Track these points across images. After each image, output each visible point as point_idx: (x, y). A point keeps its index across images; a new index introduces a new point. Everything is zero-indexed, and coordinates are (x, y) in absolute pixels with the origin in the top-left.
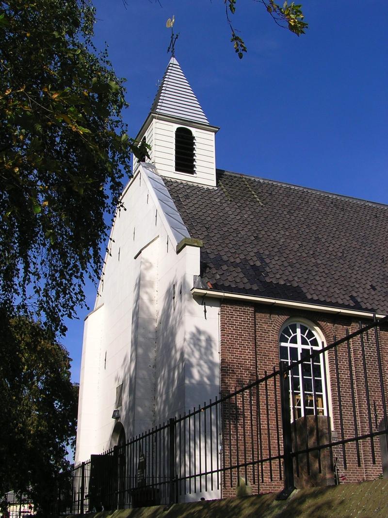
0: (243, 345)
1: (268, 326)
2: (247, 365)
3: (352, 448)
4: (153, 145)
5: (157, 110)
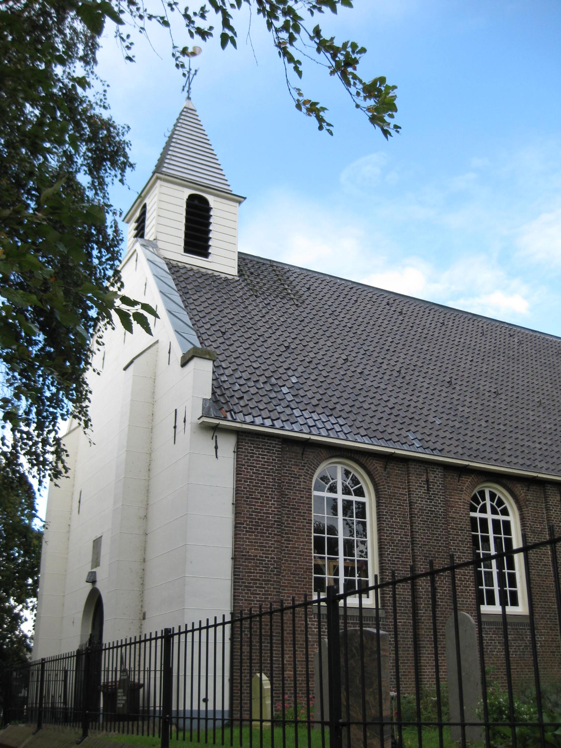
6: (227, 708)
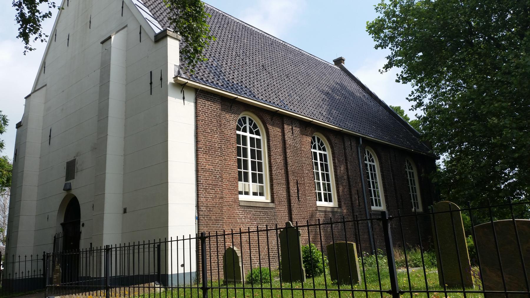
6: (194, 269)
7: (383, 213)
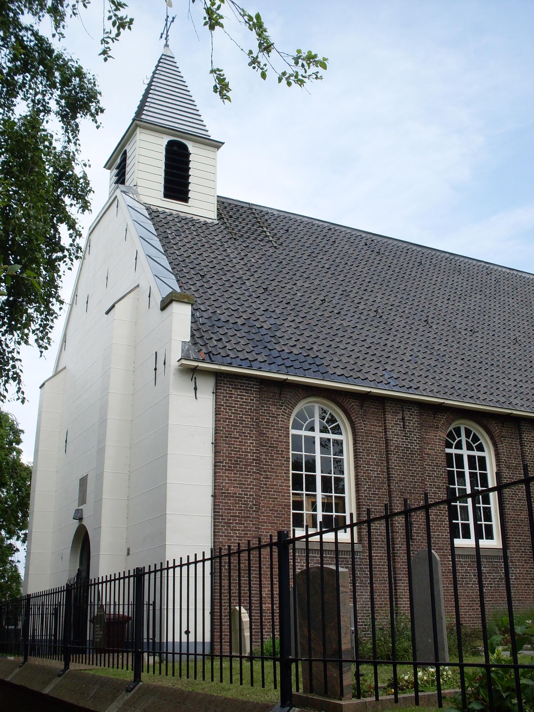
0: (244, 433)
1: (277, 408)
2: (248, 459)
3: (380, 565)
4: (136, 171)
5: (143, 117)
6: (208, 639)
7: (21, 530)
